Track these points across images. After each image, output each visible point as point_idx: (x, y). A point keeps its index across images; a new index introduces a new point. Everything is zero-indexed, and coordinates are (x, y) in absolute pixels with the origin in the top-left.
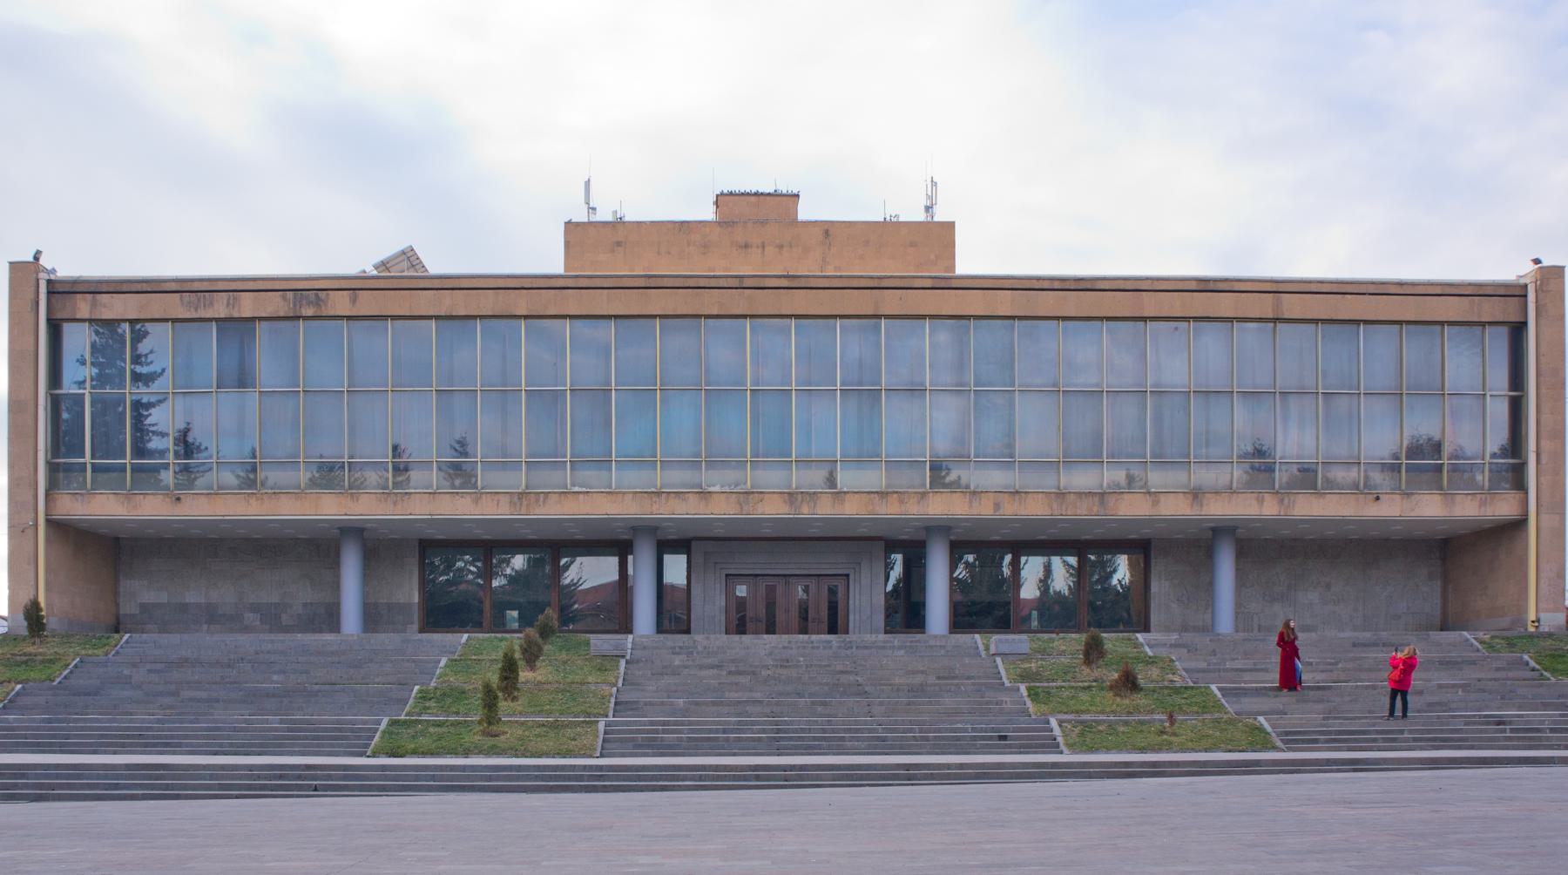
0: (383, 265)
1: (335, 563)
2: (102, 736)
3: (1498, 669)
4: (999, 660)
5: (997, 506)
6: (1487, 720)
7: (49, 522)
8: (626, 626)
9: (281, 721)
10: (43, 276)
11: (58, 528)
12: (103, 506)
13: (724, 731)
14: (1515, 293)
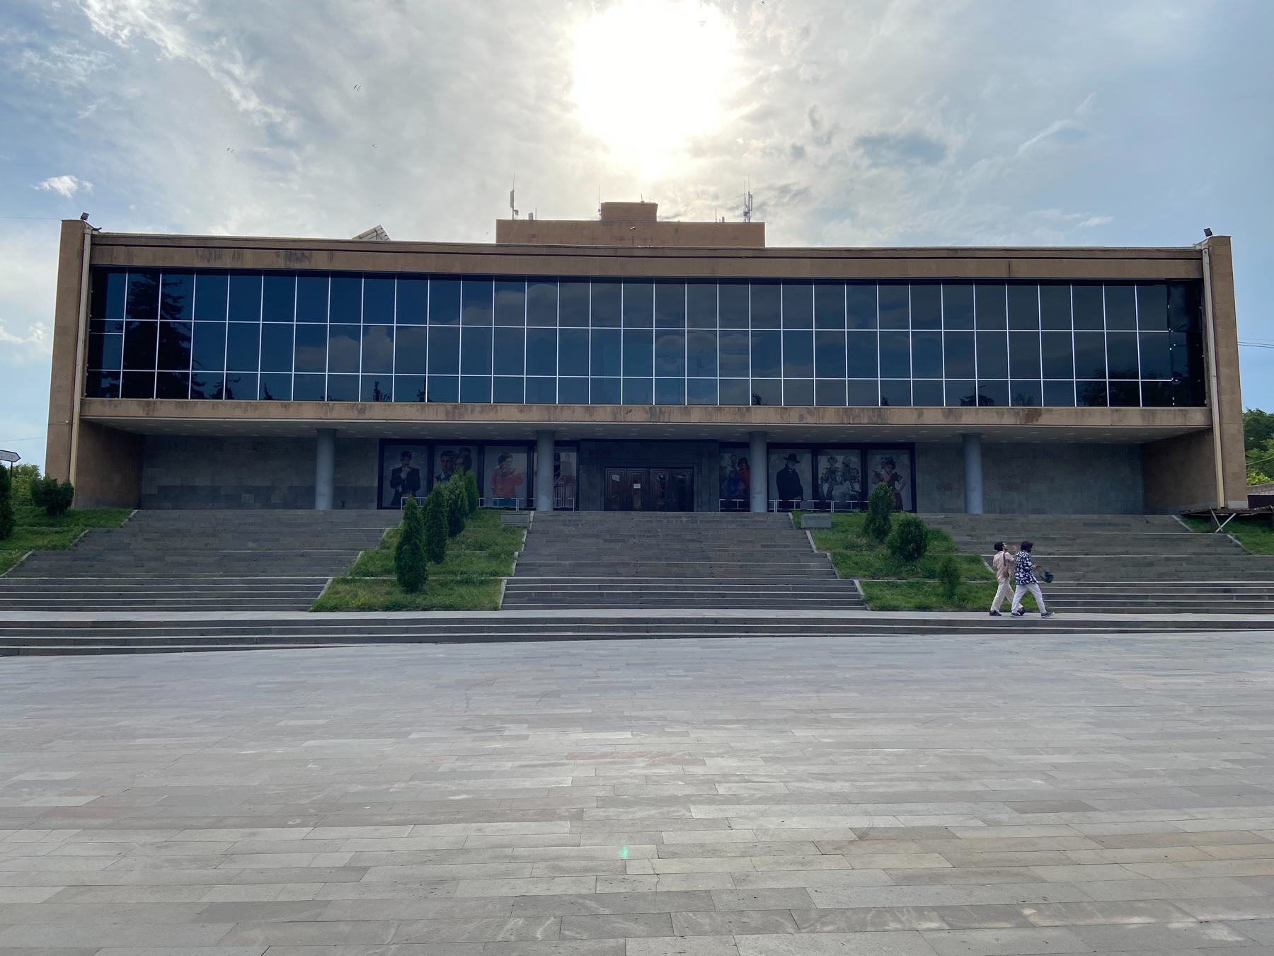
0: (360, 237)
1: (313, 457)
2: (86, 596)
3: (1208, 546)
4: (808, 533)
5: (801, 417)
6: (1215, 589)
7: (83, 422)
8: (312, 506)
9: (243, 582)
10: (88, 231)
11: (90, 426)
12: (127, 410)
13: (600, 588)
14: (1192, 256)
